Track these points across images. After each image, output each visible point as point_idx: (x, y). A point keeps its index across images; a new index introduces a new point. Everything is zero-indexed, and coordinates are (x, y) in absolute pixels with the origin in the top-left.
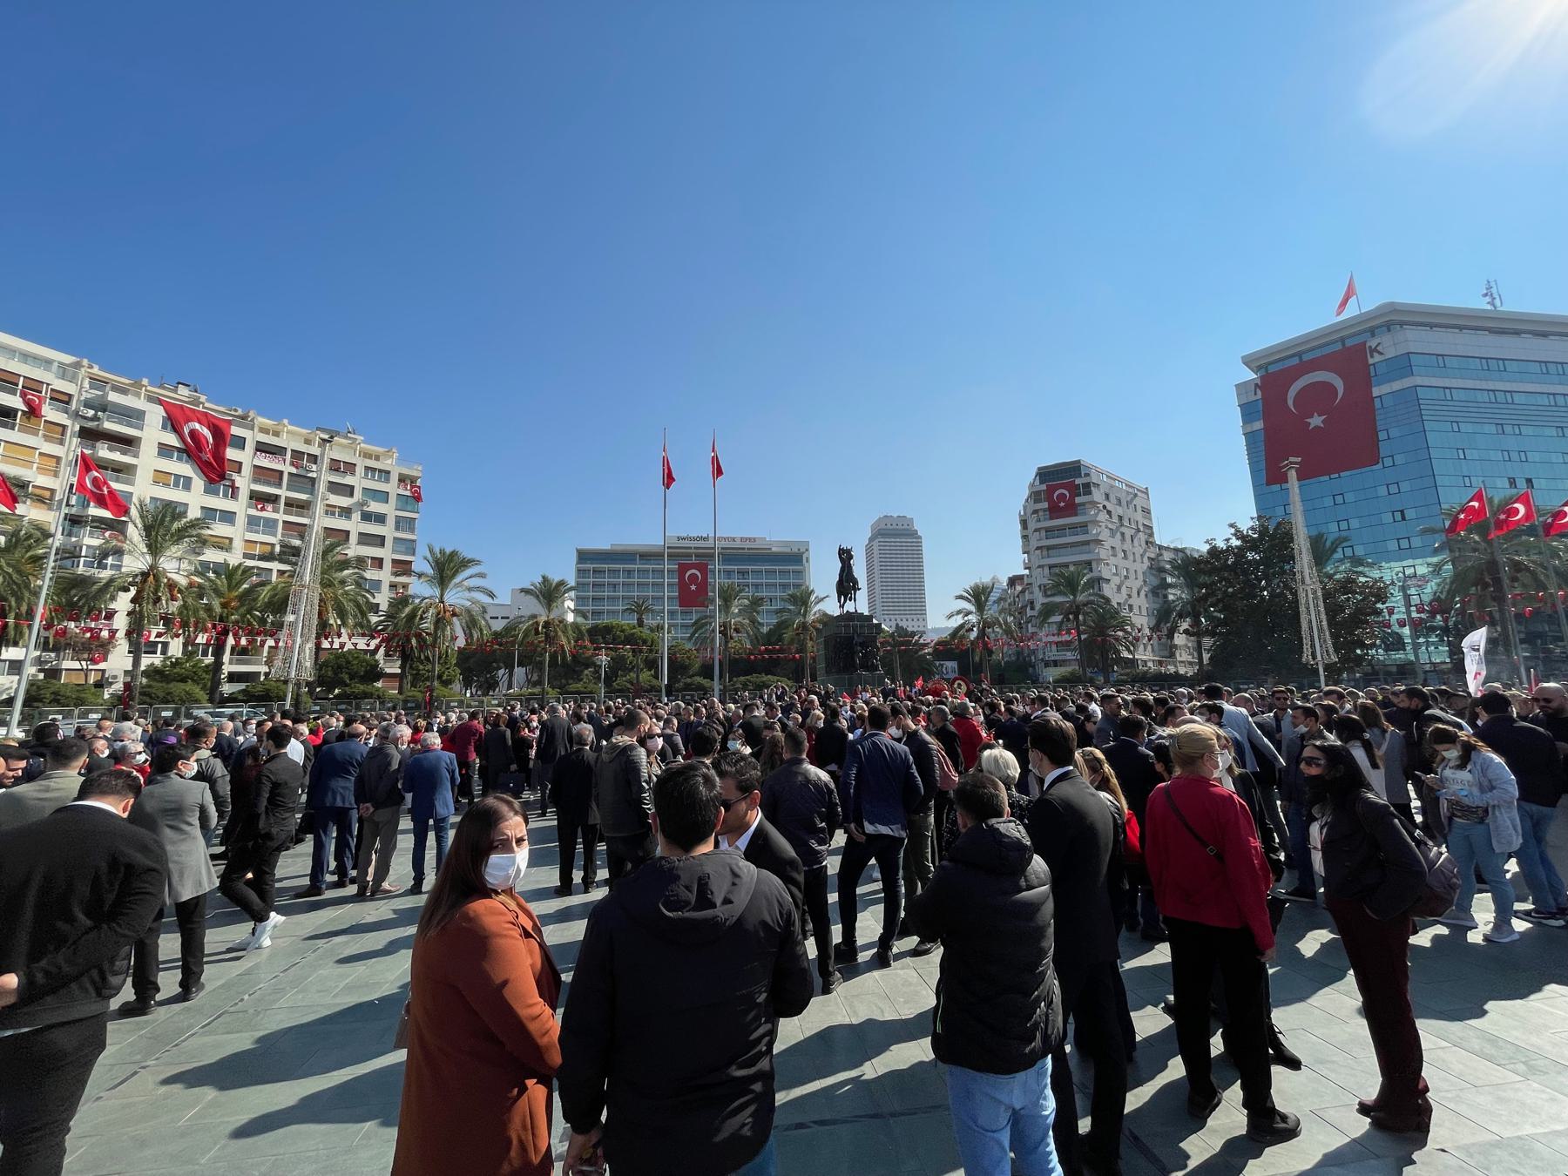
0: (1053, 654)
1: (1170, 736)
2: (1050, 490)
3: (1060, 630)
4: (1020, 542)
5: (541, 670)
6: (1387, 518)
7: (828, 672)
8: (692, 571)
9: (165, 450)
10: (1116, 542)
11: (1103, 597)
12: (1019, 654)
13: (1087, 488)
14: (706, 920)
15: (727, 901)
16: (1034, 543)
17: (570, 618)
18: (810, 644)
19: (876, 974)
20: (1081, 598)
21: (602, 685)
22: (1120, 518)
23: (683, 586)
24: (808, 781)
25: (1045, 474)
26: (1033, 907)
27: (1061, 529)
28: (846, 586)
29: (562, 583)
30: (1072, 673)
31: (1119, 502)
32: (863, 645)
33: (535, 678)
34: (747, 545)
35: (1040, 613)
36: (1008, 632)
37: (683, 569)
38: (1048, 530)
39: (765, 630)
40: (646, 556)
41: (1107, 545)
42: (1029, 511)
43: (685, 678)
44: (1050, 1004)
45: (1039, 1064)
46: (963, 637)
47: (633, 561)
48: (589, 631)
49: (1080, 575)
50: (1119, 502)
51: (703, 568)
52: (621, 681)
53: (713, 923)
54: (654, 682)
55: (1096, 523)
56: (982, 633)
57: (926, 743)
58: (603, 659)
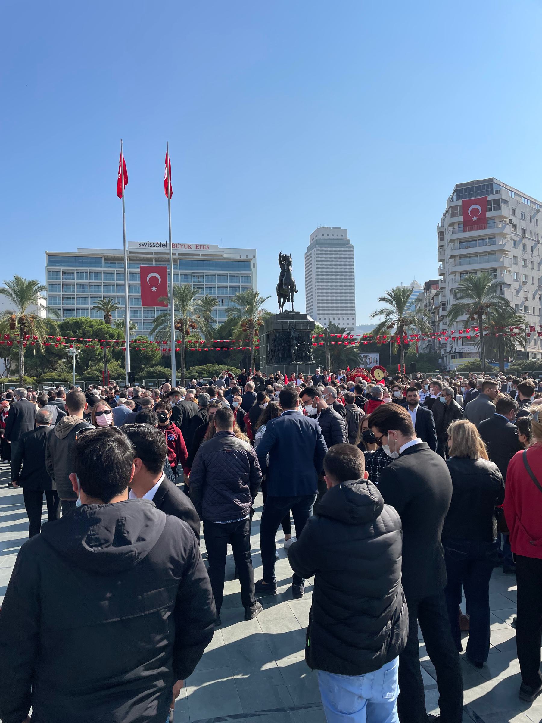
0: (458, 347)
1: (534, 412)
2: (465, 206)
3: (466, 327)
5: (18, 360)
7: (269, 362)
8: (153, 276)
10: (518, 252)
11: (503, 299)
12: (431, 347)
13: (497, 204)
14: (121, 555)
15: (140, 539)
16: (448, 253)
17: (43, 314)
18: (256, 338)
19: (290, 603)
20: (485, 300)
21: (74, 374)
22: (524, 231)
23: (145, 287)
24: (233, 450)
25: (461, 191)
26: (387, 544)
27: (472, 240)
28: (286, 288)
29: (33, 284)
30: (474, 364)
32: (299, 339)
33: (13, 367)
34: (201, 251)
35: (450, 313)
36: (422, 328)
37: (144, 272)
38: (461, 241)
39: (217, 326)
40: (112, 260)
41: (510, 255)
42: (446, 224)
43: (144, 365)
44: (396, 622)
45: (385, 667)
46: (384, 333)
47: (99, 264)
48: (61, 327)
49: (486, 280)
51: (163, 272)
52: (91, 370)
53: (130, 557)
54: (121, 370)
55: (503, 235)
56: (400, 330)
57: (336, 419)
58: (74, 351)
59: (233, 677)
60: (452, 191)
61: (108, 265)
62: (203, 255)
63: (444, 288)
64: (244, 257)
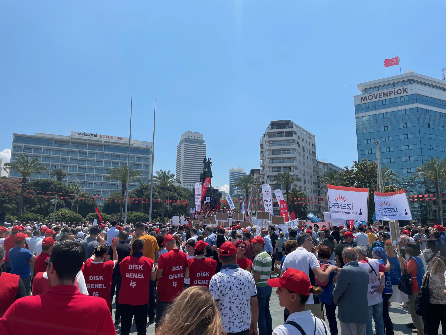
4: (259, 154)
6: (404, 159)
9: (366, 100)
22: (303, 148)
31: (303, 140)
34: (119, 141)
50: (303, 140)
59: (258, 326)
60: (269, 124)
61: (56, 145)
62: (120, 143)
63: (263, 174)
64: (145, 146)
